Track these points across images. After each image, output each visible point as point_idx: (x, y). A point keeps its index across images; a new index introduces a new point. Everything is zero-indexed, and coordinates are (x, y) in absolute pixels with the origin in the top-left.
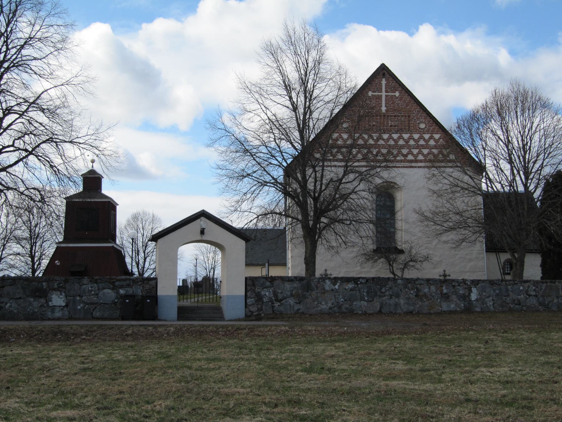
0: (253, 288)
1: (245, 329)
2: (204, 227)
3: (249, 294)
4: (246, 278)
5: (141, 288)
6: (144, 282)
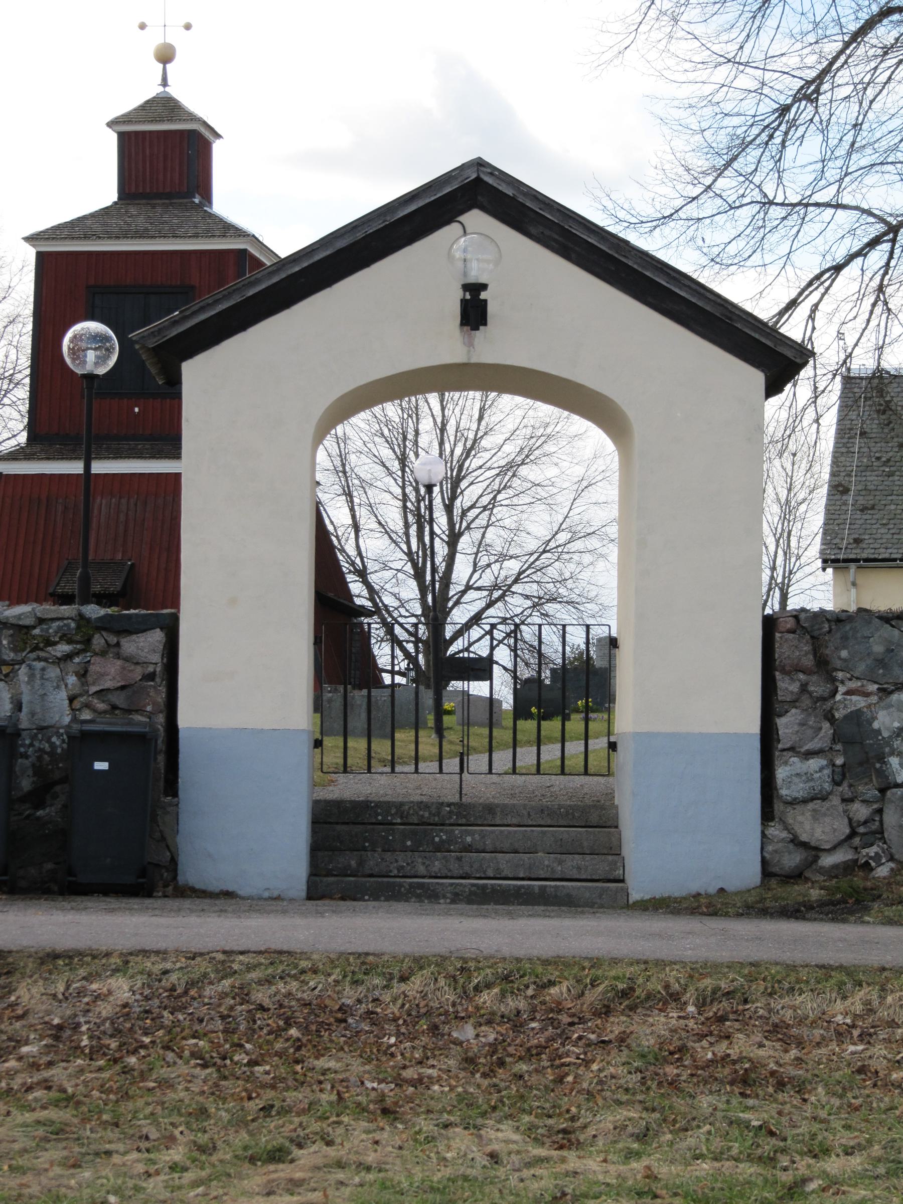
0: (818, 688)
1: (674, 998)
2: (476, 275)
3: (786, 725)
4: (769, 624)
5: (72, 680)
6: (88, 641)
